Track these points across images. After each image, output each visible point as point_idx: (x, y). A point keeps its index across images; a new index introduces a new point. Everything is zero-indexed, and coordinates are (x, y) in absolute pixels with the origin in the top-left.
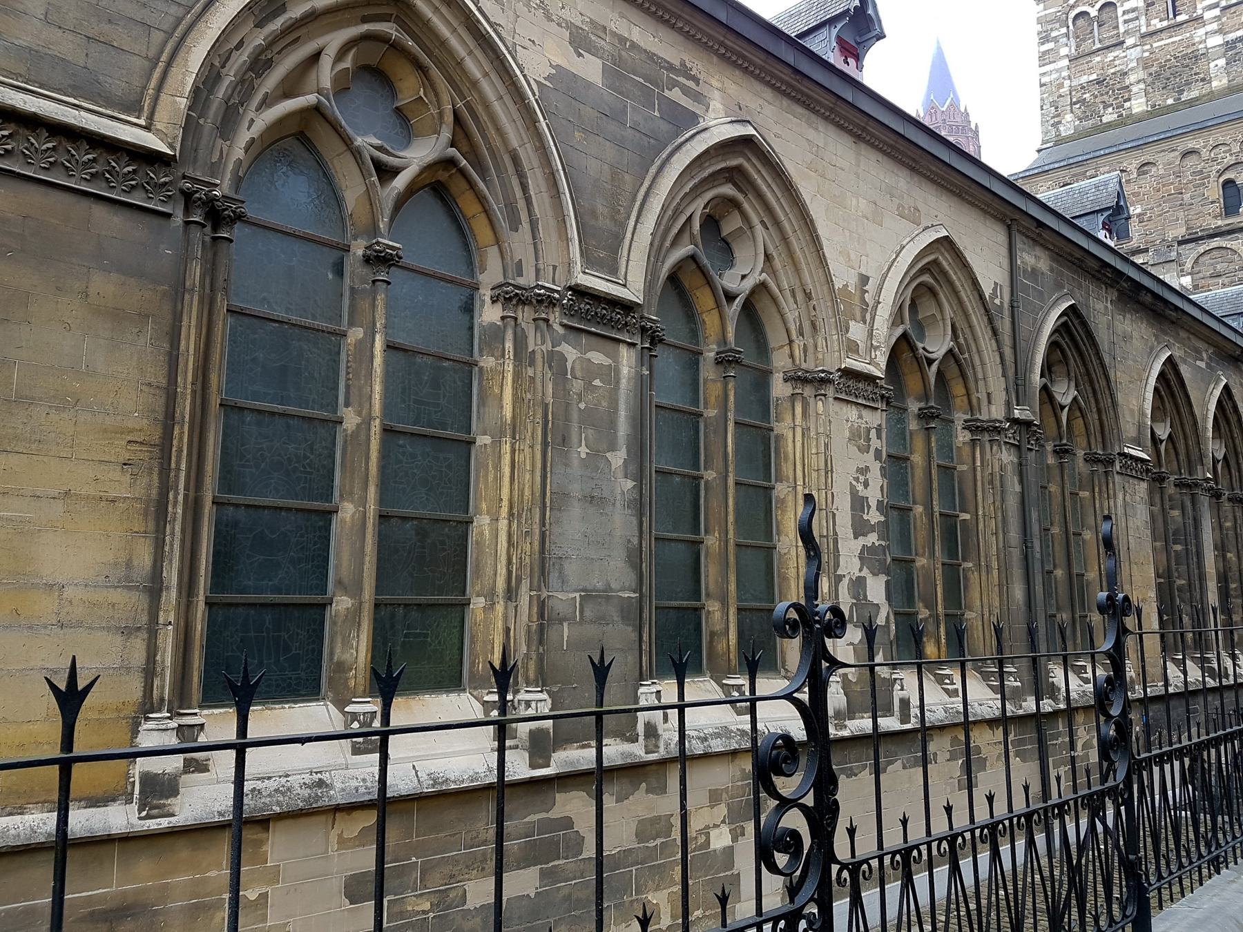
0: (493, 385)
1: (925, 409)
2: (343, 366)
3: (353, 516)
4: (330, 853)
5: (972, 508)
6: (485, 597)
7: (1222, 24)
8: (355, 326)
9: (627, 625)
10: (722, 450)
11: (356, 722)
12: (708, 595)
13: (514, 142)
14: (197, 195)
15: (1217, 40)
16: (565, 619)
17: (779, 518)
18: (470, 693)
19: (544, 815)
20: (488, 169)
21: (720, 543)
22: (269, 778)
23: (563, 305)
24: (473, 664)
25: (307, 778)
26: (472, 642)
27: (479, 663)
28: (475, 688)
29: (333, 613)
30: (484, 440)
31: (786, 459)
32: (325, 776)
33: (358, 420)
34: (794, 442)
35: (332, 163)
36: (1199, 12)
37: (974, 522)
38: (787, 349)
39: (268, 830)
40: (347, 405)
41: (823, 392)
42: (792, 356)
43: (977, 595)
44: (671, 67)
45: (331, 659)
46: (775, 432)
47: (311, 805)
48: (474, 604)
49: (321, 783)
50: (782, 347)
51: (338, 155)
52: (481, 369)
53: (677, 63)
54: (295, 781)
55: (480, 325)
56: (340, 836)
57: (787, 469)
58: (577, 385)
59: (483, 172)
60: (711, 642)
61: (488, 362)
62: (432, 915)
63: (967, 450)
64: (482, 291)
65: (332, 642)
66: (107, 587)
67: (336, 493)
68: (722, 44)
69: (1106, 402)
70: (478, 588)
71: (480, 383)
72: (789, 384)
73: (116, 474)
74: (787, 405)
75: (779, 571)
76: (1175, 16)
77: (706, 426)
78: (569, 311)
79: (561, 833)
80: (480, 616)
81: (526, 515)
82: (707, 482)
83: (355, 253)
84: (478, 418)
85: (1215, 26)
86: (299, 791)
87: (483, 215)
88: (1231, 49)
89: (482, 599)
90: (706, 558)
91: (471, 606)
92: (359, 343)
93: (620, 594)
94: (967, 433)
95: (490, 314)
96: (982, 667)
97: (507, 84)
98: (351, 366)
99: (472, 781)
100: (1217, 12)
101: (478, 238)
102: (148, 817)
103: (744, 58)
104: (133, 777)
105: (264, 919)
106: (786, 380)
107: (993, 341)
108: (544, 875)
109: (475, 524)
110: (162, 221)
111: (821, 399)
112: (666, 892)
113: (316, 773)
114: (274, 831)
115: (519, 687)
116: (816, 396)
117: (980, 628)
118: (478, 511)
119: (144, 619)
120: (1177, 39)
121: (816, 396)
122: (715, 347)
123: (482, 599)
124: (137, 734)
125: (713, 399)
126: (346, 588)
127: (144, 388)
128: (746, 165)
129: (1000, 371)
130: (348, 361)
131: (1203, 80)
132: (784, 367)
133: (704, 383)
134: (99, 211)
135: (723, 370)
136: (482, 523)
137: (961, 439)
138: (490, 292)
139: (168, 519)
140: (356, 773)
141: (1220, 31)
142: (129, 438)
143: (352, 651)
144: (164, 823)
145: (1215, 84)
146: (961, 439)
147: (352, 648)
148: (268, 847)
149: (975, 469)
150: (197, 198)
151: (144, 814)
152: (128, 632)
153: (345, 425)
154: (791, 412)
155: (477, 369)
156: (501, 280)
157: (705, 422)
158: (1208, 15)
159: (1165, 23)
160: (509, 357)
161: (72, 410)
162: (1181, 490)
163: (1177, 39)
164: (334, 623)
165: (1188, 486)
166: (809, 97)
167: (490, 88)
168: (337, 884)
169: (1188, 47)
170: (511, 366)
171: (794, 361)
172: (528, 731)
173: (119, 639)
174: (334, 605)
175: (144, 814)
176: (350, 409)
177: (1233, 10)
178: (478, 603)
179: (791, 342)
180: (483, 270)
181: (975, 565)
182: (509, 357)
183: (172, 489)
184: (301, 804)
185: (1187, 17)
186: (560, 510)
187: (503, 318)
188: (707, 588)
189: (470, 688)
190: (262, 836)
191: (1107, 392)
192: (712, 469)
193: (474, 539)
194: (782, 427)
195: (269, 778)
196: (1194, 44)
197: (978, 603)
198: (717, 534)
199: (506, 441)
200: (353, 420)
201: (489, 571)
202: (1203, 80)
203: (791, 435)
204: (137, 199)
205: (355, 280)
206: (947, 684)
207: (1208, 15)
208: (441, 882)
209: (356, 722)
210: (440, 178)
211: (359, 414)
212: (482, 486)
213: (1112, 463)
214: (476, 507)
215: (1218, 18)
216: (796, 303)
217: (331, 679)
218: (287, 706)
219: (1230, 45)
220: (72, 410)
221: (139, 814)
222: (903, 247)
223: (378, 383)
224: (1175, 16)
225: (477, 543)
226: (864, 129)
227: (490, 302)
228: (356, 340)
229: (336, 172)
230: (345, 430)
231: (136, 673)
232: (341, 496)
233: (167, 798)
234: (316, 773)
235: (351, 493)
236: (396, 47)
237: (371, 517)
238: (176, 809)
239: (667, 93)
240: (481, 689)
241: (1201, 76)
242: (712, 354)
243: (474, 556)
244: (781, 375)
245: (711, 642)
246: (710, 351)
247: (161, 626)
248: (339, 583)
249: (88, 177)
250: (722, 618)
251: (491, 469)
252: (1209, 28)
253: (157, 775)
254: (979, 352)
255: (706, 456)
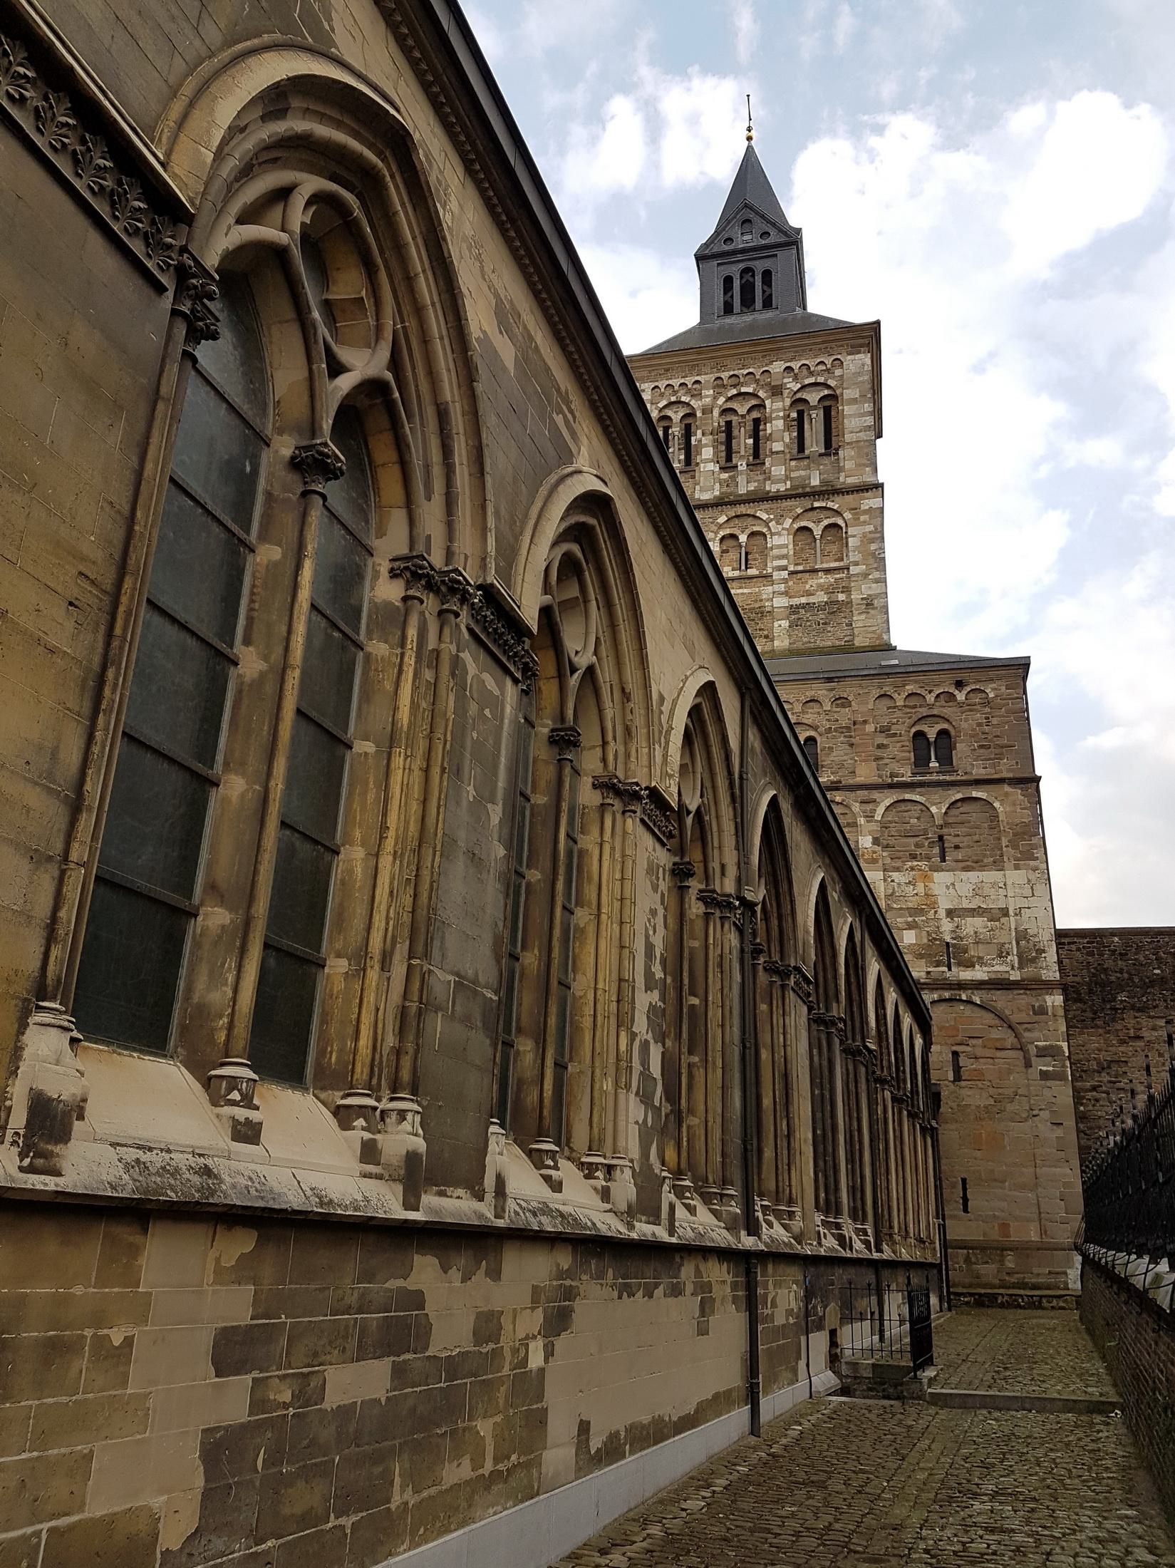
0: (383, 679)
1: (681, 864)
2: (246, 590)
3: (243, 796)
4: (206, 1287)
5: (701, 992)
6: (349, 960)
7: (789, 587)
8: (270, 543)
9: (487, 1036)
10: (550, 846)
11: (236, 1092)
12: (519, 1030)
13: (448, 396)
14: (194, 281)
15: (781, 602)
16: (441, 1009)
17: (577, 951)
18: (314, 1095)
19: (399, 1283)
20: (414, 416)
21: (539, 964)
22: (150, 1149)
23: (473, 604)
24: (322, 1053)
25: (193, 1161)
26: (324, 1021)
27: (331, 1053)
28: (323, 1089)
29: (199, 931)
30: (364, 747)
31: (590, 880)
32: (209, 1162)
33: (262, 666)
34: (600, 861)
35: (269, 329)
36: (770, 570)
37: (703, 1009)
38: (599, 751)
39: (145, 1231)
40: (247, 641)
41: (633, 808)
42: (604, 760)
43: (702, 1098)
44: (558, 390)
45: (187, 998)
46: (579, 846)
47: (207, 1198)
48: (330, 967)
49: (207, 1171)
50: (594, 747)
51: (280, 322)
52: (368, 657)
53: (563, 389)
54: (181, 1160)
55: (371, 601)
56: (218, 1260)
57: (590, 892)
58: (473, 708)
59: (410, 417)
60: (519, 1090)
61: (379, 649)
62: (291, 1411)
63: (699, 924)
64: (377, 559)
65: (192, 970)
66: (25, 778)
67: (220, 758)
68: (597, 390)
69: (787, 908)
70: (338, 945)
71: (365, 672)
72: (598, 792)
73: (58, 611)
74: (595, 816)
75: (572, 1019)
76: (747, 568)
77: (532, 815)
78: (475, 612)
79: (414, 1313)
80: (339, 985)
81: (409, 856)
82: (529, 885)
83: (277, 452)
84: (359, 716)
85: (782, 587)
86: (187, 1176)
87: (396, 468)
88: (794, 613)
89: (344, 963)
90: (521, 981)
91: (327, 970)
92: (273, 566)
93: (484, 991)
94: (700, 904)
95: (388, 591)
96: (702, 1187)
97: (449, 325)
98: (259, 594)
99: (355, 1210)
100: (785, 574)
101: (382, 493)
102: (31, 1170)
103: (610, 415)
104: (11, 1099)
105: (124, 1384)
106: (595, 786)
107: (731, 809)
108: (399, 1372)
109: (342, 856)
110: (148, 291)
111: (630, 816)
112: (492, 1421)
113: (200, 1155)
114: (152, 1235)
115: (382, 1094)
116: (624, 812)
117: (703, 1138)
118: (348, 840)
119: (59, 846)
120: (745, 591)
121: (624, 812)
122: (550, 722)
123: (344, 962)
124: (25, 1029)
125: (543, 784)
126: (222, 896)
127: (105, 505)
128: (598, 527)
129: (734, 843)
130: (254, 586)
131: (766, 637)
132: (593, 771)
133: (534, 762)
134: (95, 240)
135: (557, 751)
136: (353, 857)
137: (694, 911)
138: (388, 562)
139: (103, 707)
140: (241, 1166)
141: (786, 593)
142: (82, 568)
143: (224, 988)
144: (46, 1183)
145: (776, 643)
146: (694, 911)
147: (226, 984)
148: (143, 1261)
149: (707, 947)
150: (193, 284)
151: (27, 1161)
152: (37, 858)
153: (241, 669)
154: (599, 825)
155: (361, 654)
156: (405, 551)
157: (532, 809)
158: (776, 575)
159: (737, 573)
160: (412, 649)
161: (27, 495)
162: (818, 1026)
163: (745, 591)
164: (197, 945)
165: (825, 1023)
166: (644, 485)
167: (436, 323)
168: (205, 1341)
169: (756, 601)
170: (413, 659)
171: (606, 766)
172: (404, 1153)
173: (25, 866)
174: (200, 918)
175: (27, 1161)
176: (251, 649)
177: (799, 576)
178: (337, 967)
179: (604, 744)
180: (381, 533)
181: (701, 1060)
182: (412, 649)
183: (111, 665)
184: (197, 1195)
185: (757, 573)
186: (448, 858)
187: (405, 599)
188: (518, 1020)
189: (315, 1088)
190: (138, 1239)
191: (788, 898)
192: (537, 869)
193: (339, 877)
194: (588, 842)
195: (150, 1149)
196: (761, 600)
197: (702, 1107)
198: (536, 951)
199: (400, 753)
200: (255, 665)
201: (358, 923)
202: (766, 637)
203: (597, 852)
204: (137, 246)
205: (274, 484)
206: (688, 1198)
207: (776, 575)
208: (306, 1361)
209: (236, 1092)
210: (358, 405)
211: (265, 658)
212: (356, 806)
213: (788, 976)
214: (345, 834)
215: (785, 581)
216: (613, 701)
217: (184, 1029)
218: (135, 1055)
219: (794, 609)
220: (27, 495)
221: (21, 1161)
222: (687, 678)
223: (302, 622)
224: (747, 568)
225: (343, 882)
226: (673, 540)
227: (387, 574)
228: (269, 561)
229: (271, 342)
230: (239, 676)
231: (38, 928)
232: (226, 764)
233: (56, 1144)
234: (200, 1155)
235: (243, 764)
236: (351, 226)
237: (278, 800)
238: (65, 1166)
239: (554, 415)
240: (332, 1089)
241: (766, 633)
242: (546, 731)
243: (337, 900)
244: (590, 780)
245: (519, 1090)
246: (544, 726)
247: (72, 866)
248: (212, 887)
249: (96, 189)
250: (535, 1061)
251: (371, 785)
252: (776, 588)
253: (50, 1100)
254: (717, 817)
255: (529, 850)
